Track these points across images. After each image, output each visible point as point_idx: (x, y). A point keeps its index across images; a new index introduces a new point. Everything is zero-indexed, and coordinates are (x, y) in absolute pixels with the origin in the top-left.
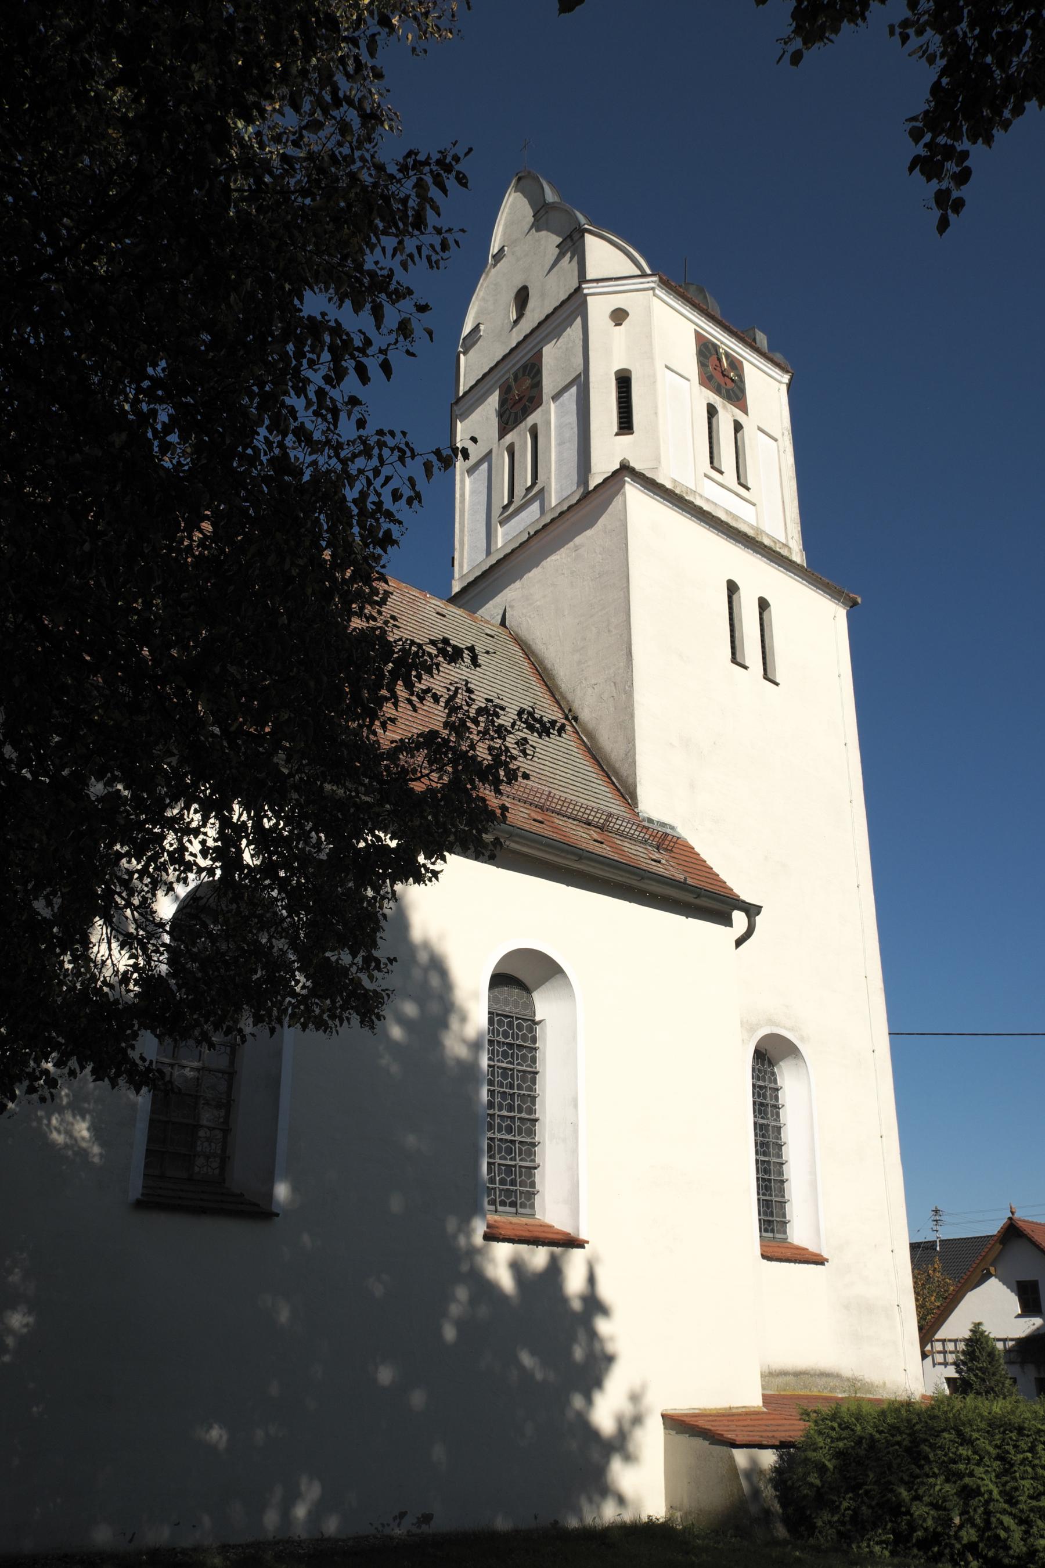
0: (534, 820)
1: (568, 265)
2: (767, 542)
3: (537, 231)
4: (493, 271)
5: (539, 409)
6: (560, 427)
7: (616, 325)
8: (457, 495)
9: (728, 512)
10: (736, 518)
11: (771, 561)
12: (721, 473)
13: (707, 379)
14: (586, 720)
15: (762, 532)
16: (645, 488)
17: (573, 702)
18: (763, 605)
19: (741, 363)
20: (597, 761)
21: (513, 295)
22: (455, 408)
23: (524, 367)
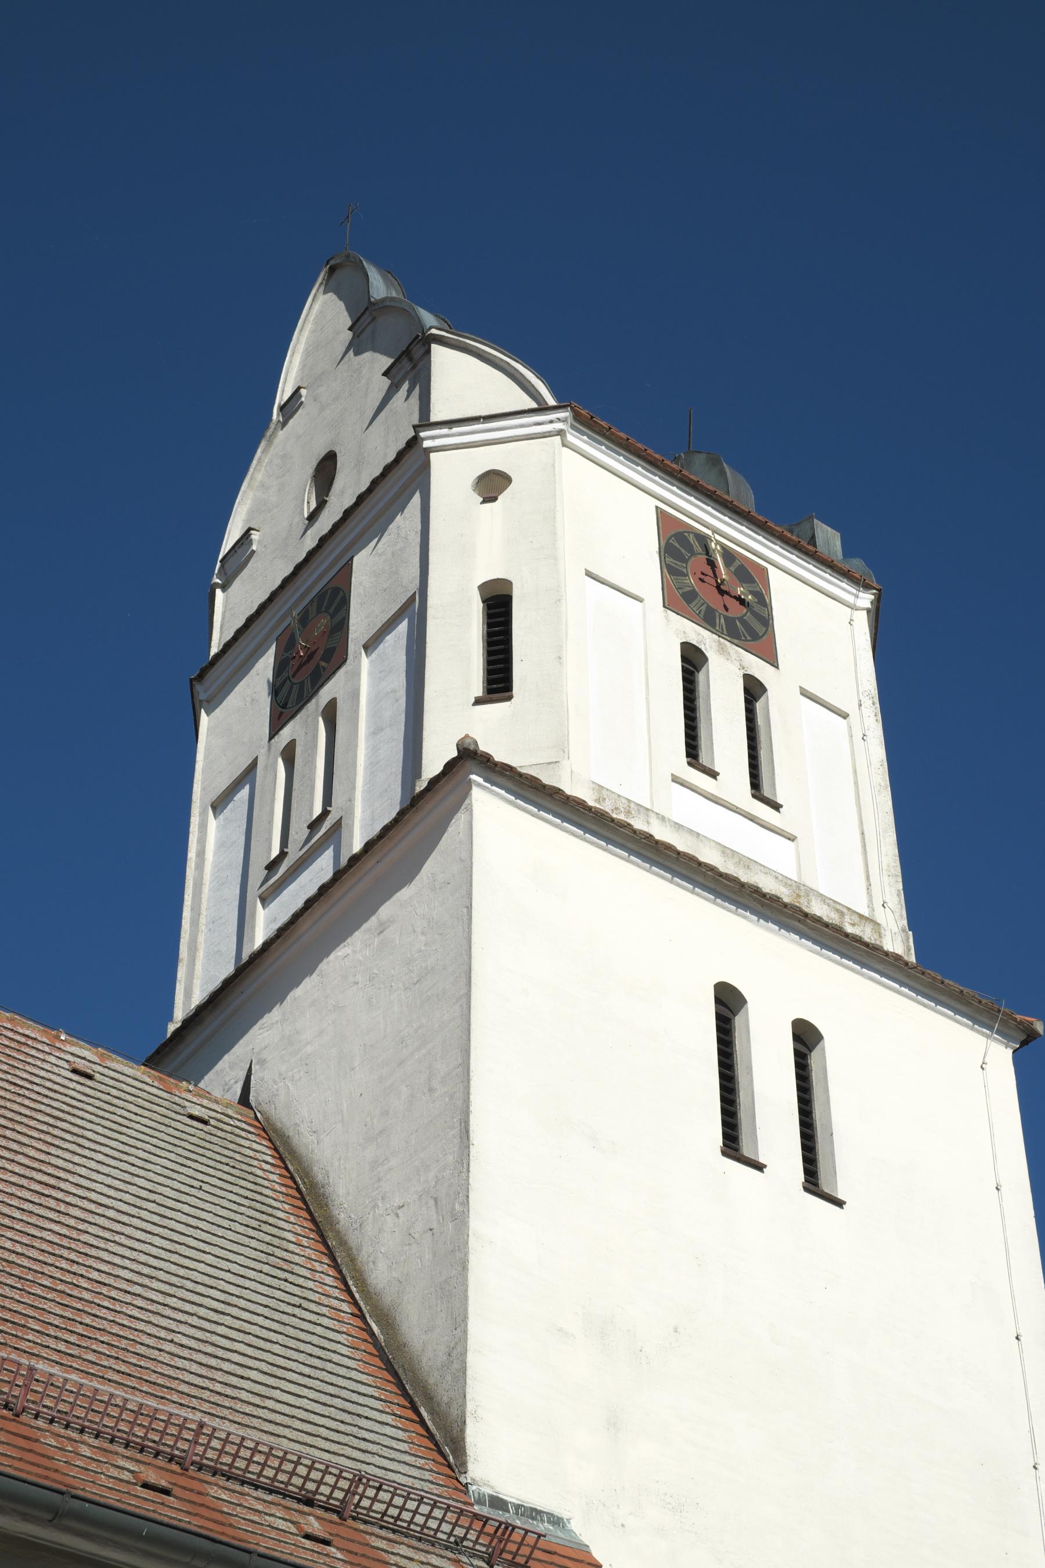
0: (146, 1486)
1: (404, 407)
2: (818, 909)
3: (356, 354)
4: (281, 434)
5: (341, 672)
6: (376, 700)
7: (486, 500)
8: (192, 854)
9: (725, 851)
10: (748, 863)
11: (823, 946)
12: (714, 775)
13: (679, 598)
14: (380, 1286)
15: (810, 891)
16: (518, 796)
17: (359, 1250)
18: (805, 1038)
19: (764, 572)
20: (395, 1374)
21: (310, 470)
22: (198, 687)
23: (321, 596)
